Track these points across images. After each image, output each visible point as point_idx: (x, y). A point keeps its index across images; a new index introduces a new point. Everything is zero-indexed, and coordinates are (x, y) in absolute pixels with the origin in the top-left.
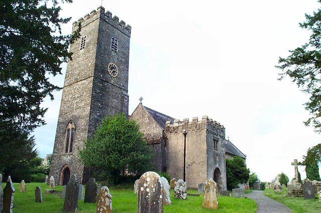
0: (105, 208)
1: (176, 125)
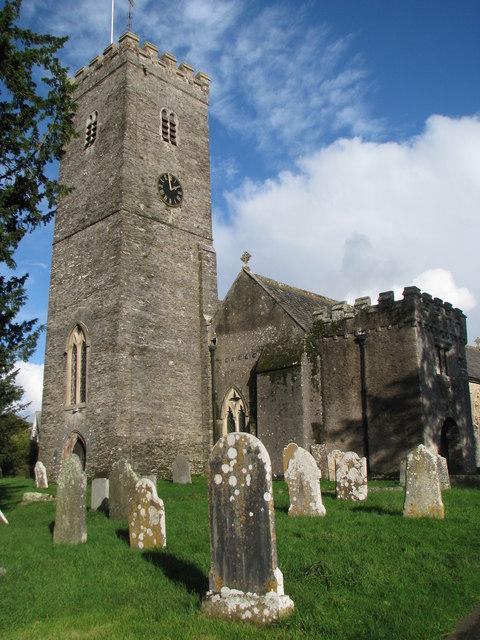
0: (149, 531)
1: (337, 316)
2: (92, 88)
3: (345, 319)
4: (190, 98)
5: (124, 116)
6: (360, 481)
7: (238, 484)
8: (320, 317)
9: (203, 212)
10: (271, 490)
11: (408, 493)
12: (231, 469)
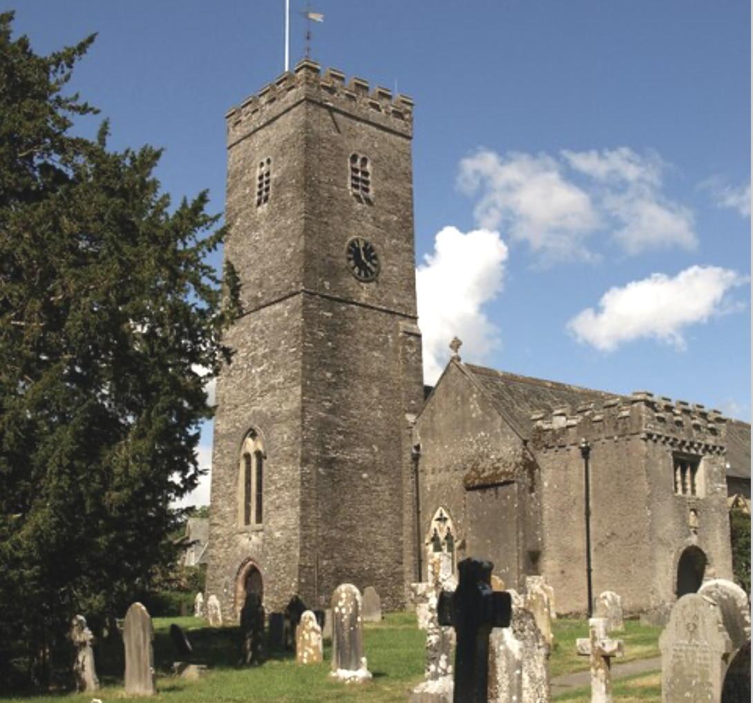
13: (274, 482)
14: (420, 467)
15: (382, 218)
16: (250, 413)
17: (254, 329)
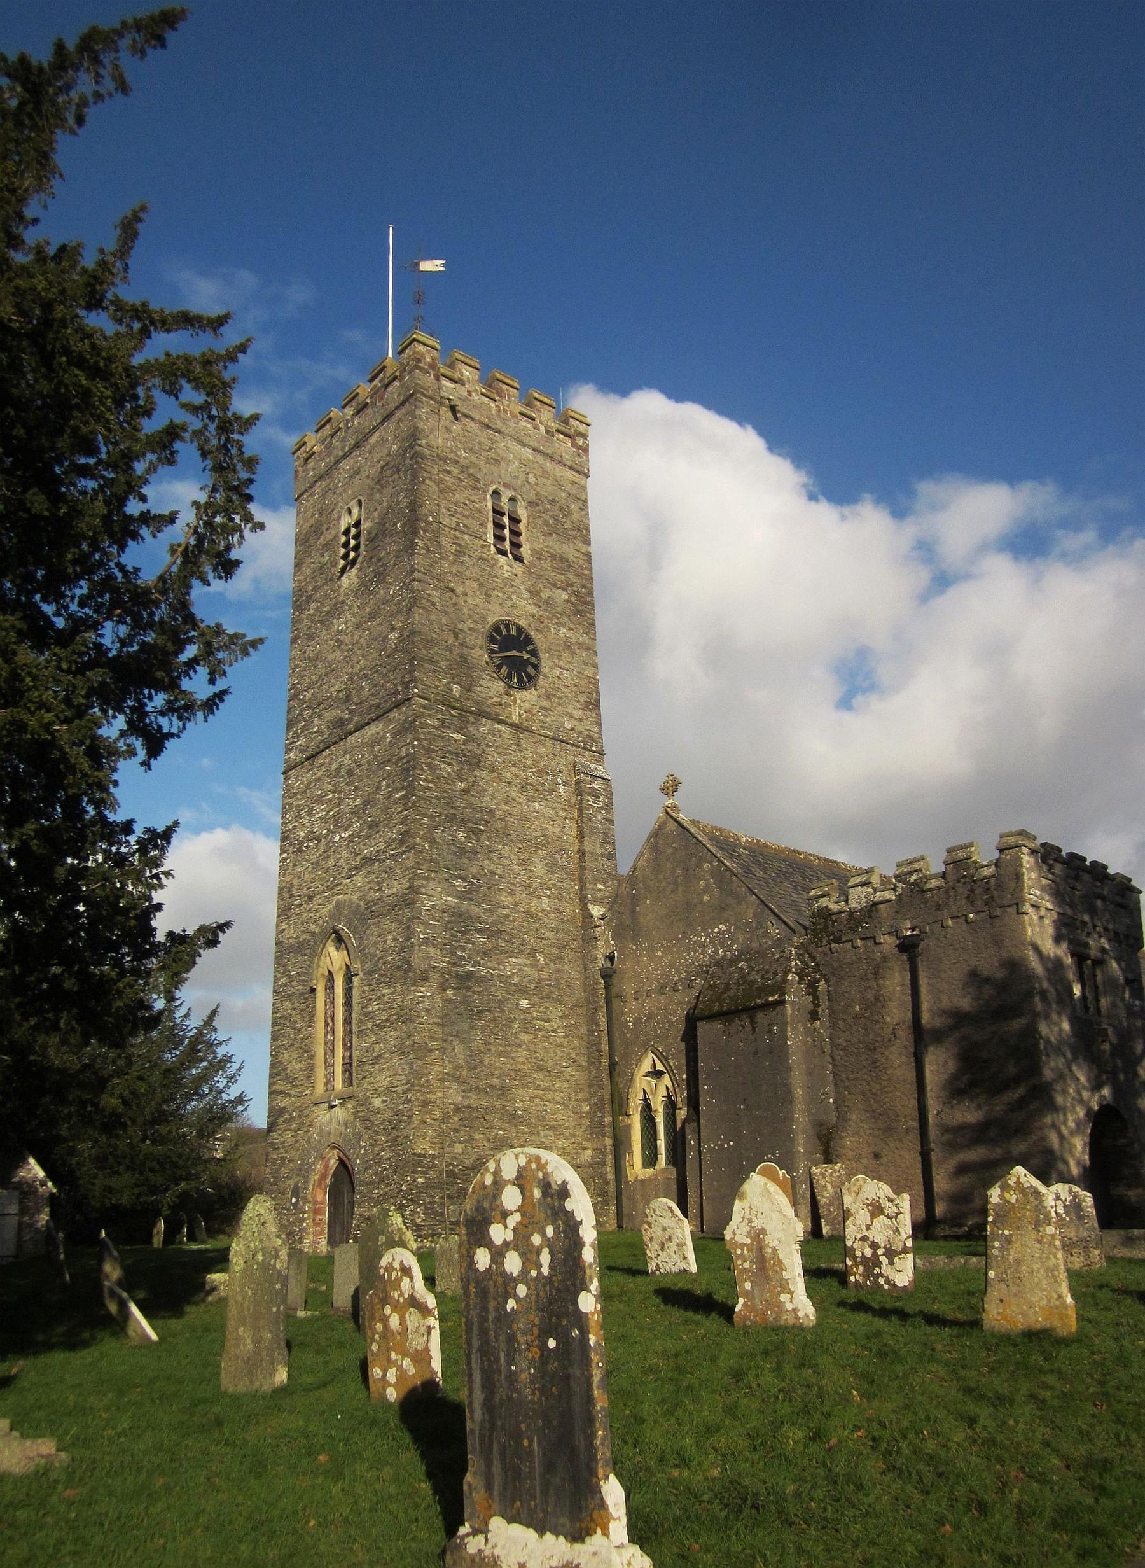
1: (858, 898)
2: (350, 453)
3: (875, 904)
4: (549, 465)
5: (414, 506)
6: (898, 1246)
7: (524, 1272)
8: (824, 902)
9: (583, 698)
10: (594, 1286)
11: (991, 1274)
12: (509, 1236)
13: (371, 1016)
14: (614, 990)
15: (545, 595)
16: (330, 906)
17: (338, 769)
